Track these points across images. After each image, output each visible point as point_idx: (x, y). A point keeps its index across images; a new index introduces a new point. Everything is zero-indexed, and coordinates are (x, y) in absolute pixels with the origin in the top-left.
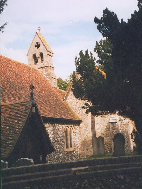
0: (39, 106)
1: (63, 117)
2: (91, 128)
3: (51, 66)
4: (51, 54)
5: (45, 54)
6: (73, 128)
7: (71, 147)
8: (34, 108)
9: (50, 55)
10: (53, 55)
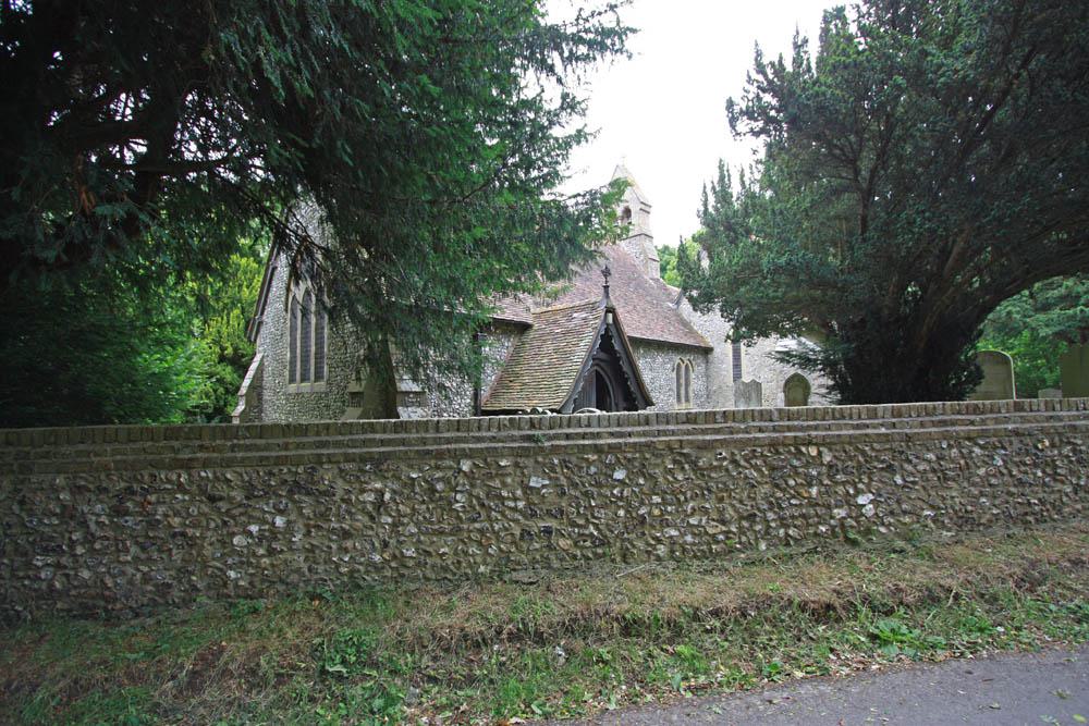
0: (620, 311)
1: (672, 339)
2: (731, 364)
3: (648, 233)
4: (647, 209)
5: (634, 208)
6: (694, 363)
7: (687, 400)
8: (610, 315)
9: (645, 209)
10: (651, 210)
